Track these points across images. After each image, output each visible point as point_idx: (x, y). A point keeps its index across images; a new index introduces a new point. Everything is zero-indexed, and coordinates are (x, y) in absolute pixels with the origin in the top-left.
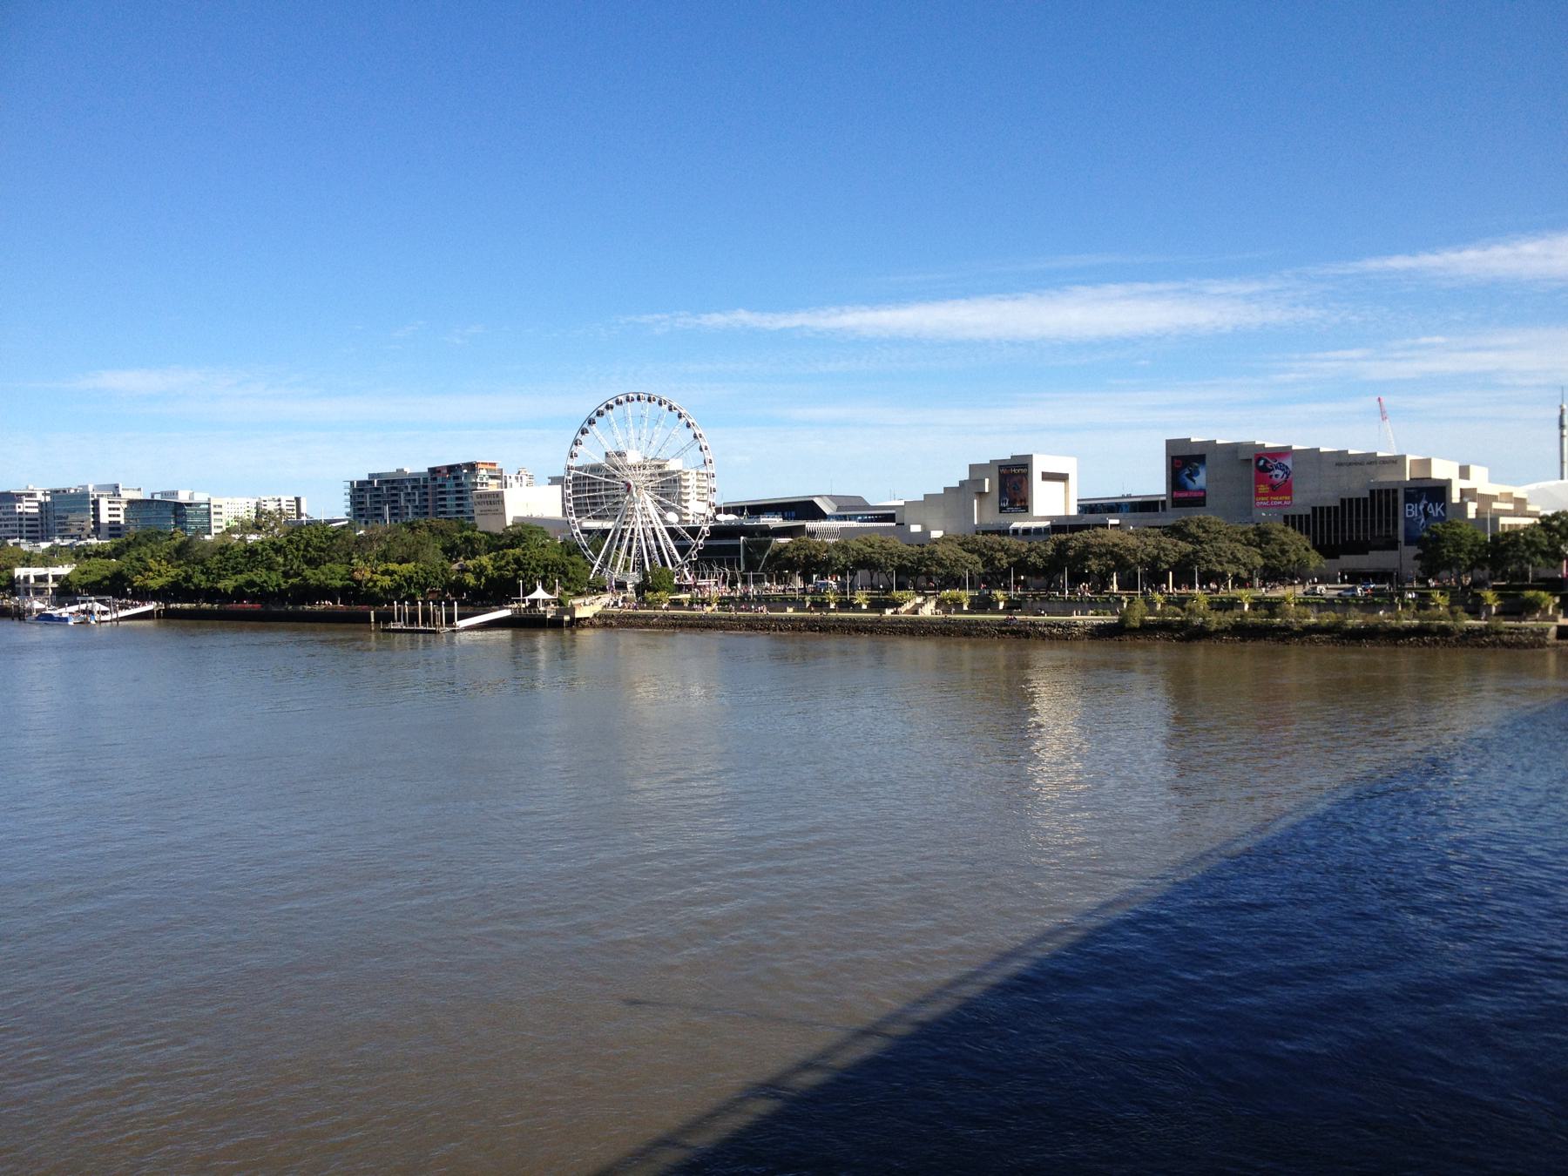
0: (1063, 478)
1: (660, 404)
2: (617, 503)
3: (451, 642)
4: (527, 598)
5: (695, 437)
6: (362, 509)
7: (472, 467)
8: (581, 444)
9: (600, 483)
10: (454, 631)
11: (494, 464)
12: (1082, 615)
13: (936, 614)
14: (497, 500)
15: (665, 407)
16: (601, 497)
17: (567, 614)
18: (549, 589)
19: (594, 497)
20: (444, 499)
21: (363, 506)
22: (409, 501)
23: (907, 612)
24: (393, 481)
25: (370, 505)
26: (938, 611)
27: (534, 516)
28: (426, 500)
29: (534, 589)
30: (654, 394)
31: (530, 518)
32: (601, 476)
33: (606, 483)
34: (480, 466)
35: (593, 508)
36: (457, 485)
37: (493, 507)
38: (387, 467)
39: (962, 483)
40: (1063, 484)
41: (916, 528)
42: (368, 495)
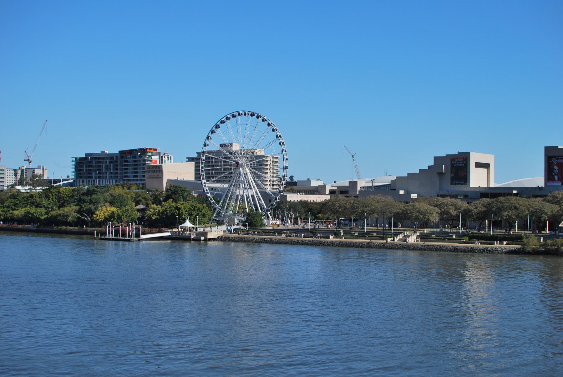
0: (486, 166)
1: (257, 117)
2: (230, 173)
3: (138, 247)
4: (179, 226)
5: (277, 137)
6: (80, 174)
7: (144, 151)
8: (211, 139)
9: (221, 162)
10: (139, 240)
11: (156, 150)
12: (500, 244)
13: (417, 241)
14: (158, 170)
15: (260, 119)
16: (221, 169)
17: (203, 236)
18: (193, 221)
19: (218, 169)
20: (127, 169)
21: (81, 172)
22: (107, 169)
23: (400, 240)
24: (99, 158)
25: (86, 171)
26: (418, 240)
27: (179, 179)
28: (155, 171)
29: (184, 221)
30: (254, 111)
31: (176, 181)
32: (222, 158)
33: (225, 162)
34: (148, 150)
35: (216, 175)
36: (135, 161)
37: (156, 174)
38: (96, 150)
39: (429, 167)
40: (487, 169)
41: (402, 192)
42: (85, 165)
